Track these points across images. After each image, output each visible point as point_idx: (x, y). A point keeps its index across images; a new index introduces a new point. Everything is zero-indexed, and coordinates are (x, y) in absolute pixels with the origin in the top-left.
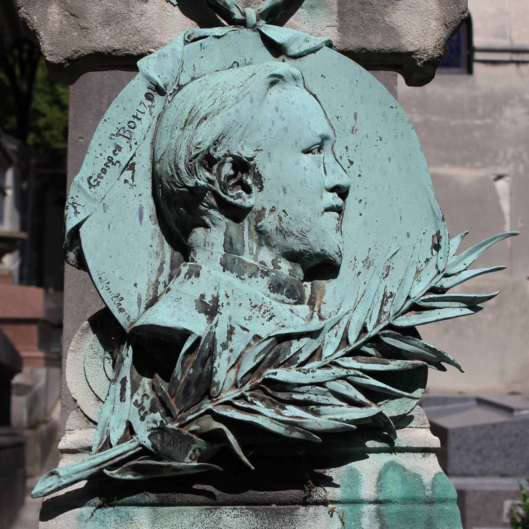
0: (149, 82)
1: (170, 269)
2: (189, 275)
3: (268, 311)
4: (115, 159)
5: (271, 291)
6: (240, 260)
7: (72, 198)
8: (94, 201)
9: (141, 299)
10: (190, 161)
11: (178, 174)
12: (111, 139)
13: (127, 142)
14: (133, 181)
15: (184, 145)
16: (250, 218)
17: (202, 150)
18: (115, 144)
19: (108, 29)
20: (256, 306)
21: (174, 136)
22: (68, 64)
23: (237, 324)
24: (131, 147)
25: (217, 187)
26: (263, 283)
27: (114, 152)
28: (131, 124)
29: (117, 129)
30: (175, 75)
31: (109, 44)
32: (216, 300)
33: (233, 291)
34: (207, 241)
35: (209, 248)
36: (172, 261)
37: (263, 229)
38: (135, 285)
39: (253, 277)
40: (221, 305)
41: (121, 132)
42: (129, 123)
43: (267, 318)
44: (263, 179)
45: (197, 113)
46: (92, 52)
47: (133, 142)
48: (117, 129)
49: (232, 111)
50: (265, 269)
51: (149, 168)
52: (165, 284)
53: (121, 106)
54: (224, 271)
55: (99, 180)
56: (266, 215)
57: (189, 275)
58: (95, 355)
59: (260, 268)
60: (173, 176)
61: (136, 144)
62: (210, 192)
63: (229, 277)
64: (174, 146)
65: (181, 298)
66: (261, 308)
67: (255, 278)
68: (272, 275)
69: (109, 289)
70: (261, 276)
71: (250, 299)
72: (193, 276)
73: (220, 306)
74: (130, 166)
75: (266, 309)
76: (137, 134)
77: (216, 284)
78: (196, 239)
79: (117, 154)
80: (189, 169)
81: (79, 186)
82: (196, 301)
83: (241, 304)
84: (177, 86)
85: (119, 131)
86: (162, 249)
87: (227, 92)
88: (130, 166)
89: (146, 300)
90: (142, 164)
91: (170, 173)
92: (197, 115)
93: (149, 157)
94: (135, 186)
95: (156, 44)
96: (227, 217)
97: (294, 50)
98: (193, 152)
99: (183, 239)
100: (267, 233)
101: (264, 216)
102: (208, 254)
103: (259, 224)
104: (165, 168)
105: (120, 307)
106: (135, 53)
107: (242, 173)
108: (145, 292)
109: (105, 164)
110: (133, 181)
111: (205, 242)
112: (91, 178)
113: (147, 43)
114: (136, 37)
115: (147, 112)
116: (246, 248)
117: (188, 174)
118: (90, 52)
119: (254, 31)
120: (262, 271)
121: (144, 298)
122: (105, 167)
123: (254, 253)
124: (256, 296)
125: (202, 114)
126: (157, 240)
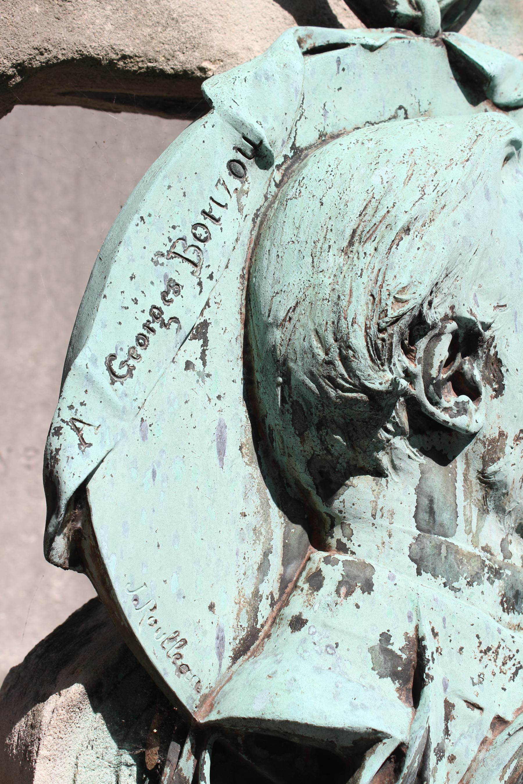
0: (239, 136)
1: (283, 564)
2: (347, 586)
3: (510, 659)
4: (168, 313)
5: (504, 611)
6: (449, 546)
7: (71, 407)
8: (121, 413)
9: (223, 639)
10: (381, 330)
11: (345, 360)
12: (156, 263)
13: (193, 273)
14: (204, 364)
15: (362, 290)
16: (471, 455)
17: (410, 305)
18: (166, 276)
19: (109, 8)
20: (489, 649)
21: (323, 266)
22: (18, 79)
23: (460, 697)
24: (200, 284)
25: (419, 390)
26: (492, 592)
27: (164, 295)
28: (200, 231)
29: (170, 240)
30: (290, 124)
31: (112, 42)
32: (418, 645)
33: (444, 620)
34: (379, 507)
35: (385, 522)
36: (285, 546)
37: (497, 478)
38: (212, 607)
39: (475, 584)
40: (430, 658)
41: (179, 249)
42: (195, 226)
43: (509, 674)
44: (503, 369)
45: (384, 217)
46: (77, 56)
47: (205, 273)
48: (170, 240)
49: (459, 216)
50: (495, 562)
51: (237, 334)
52: (272, 598)
53: (176, 186)
54: (419, 573)
55: (131, 362)
56: (508, 450)
57: (347, 586)
58: (97, 762)
59: (487, 562)
60: (330, 363)
61: (211, 277)
62: (402, 399)
63: (429, 586)
64: (328, 291)
65: (337, 645)
66: (497, 653)
67: (478, 584)
68: (507, 575)
69: (156, 622)
70: (489, 578)
71: (478, 636)
72: (358, 591)
73: (428, 661)
74: (200, 331)
75: (508, 653)
76: (214, 253)
77: (410, 607)
78: (355, 500)
79: (171, 301)
80: (377, 349)
81: (89, 378)
82: (371, 650)
83: (461, 649)
84: (292, 148)
85: (173, 246)
86: (266, 520)
87: (442, 172)
88: (200, 331)
89: (234, 639)
90: (223, 325)
91: (322, 355)
92: (387, 222)
93: (238, 309)
94: (208, 375)
95: (214, 53)
96: (424, 451)
97: (506, 92)
98: (389, 308)
99: (317, 500)
100: (506, 486)
101: (502, 450)
102: (381, 534)
103: (492, 468)
104: (300, 340)
105: (179, 663)
106: (168, 69)
107: (463, 356)
108: (233, 622)
109: (144, 326)
110: (204, 364)
111: (375, 509)
112: (113, 357)
113: (194, 47)
114: (171, 33)
115: (232, 204)
116: (461, 520)
117: (372, 360)
118: (70, 55)
119: (437, 44)
120: (490, 568)
121: (229, 635)
122: (145, 332)
123: (474, 529)
124: (487, 627)
125: (402, 221)
126: (255, 500)
